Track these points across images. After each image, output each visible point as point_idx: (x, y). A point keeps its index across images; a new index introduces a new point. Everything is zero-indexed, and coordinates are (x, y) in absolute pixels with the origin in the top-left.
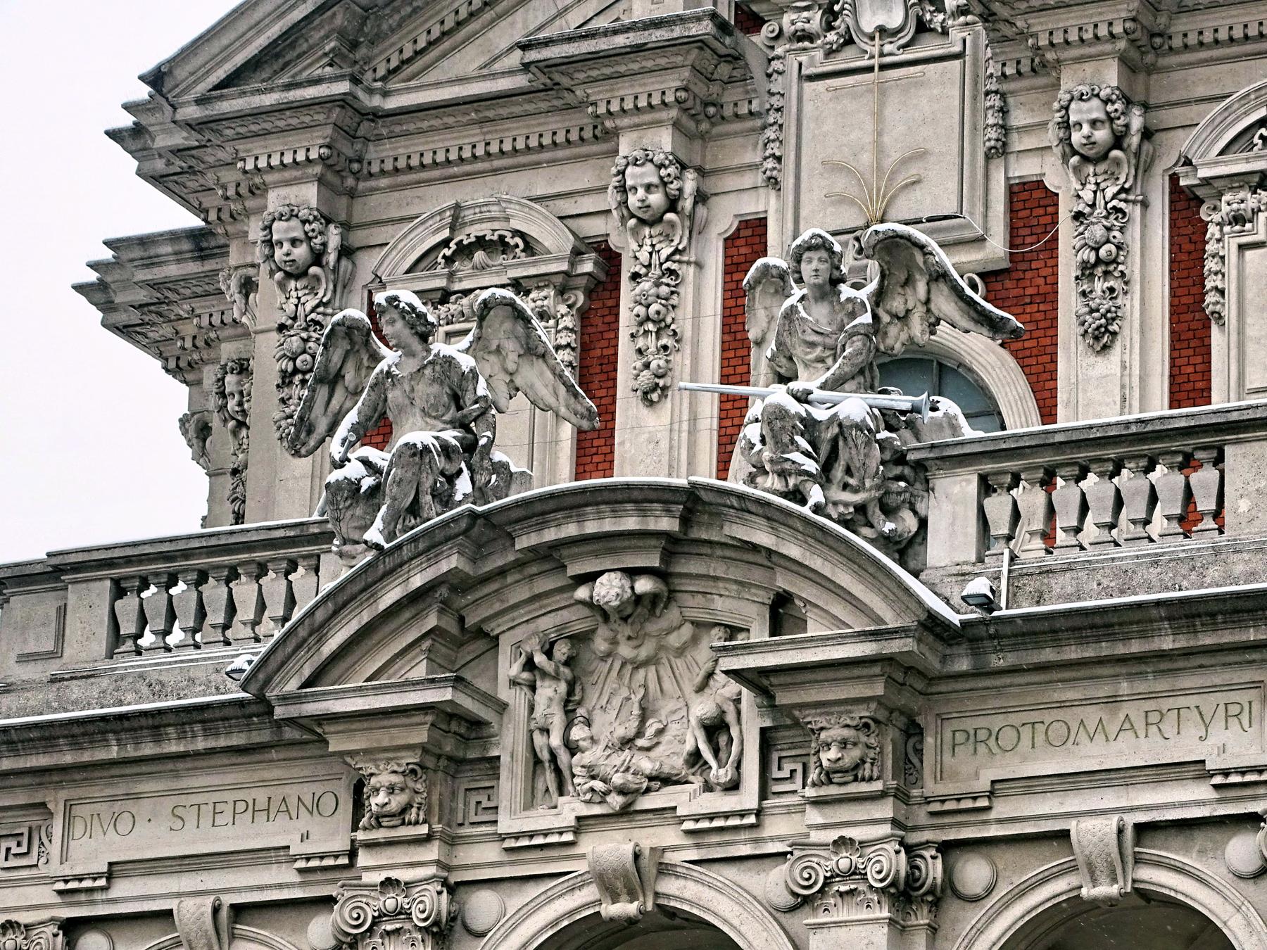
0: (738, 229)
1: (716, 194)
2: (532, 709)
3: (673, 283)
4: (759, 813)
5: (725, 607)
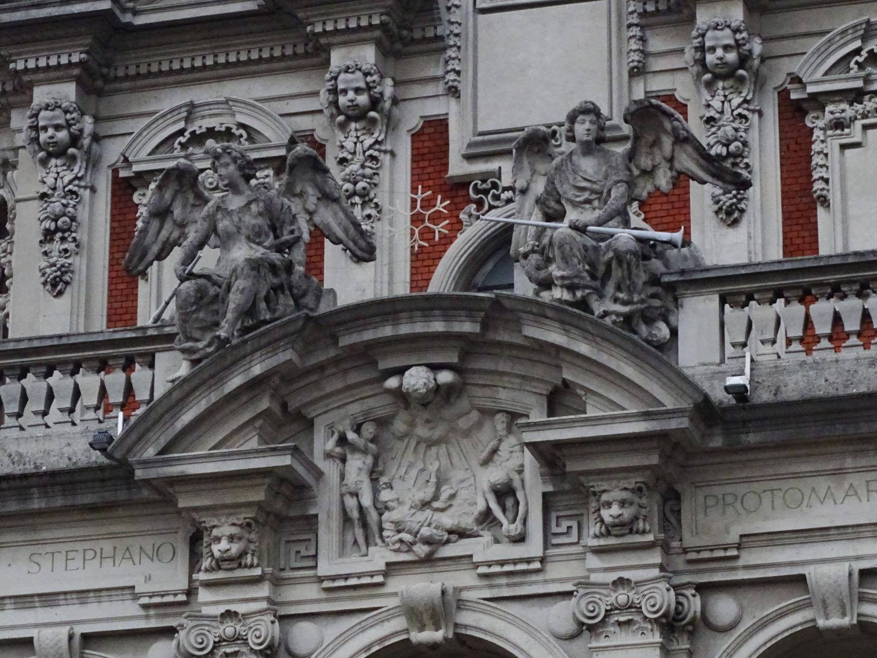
0: (422, 128)
1: (405, 100)
2: (342, 477)
3: (374, 166)
4: (543, 560)
5: (506, 397)
